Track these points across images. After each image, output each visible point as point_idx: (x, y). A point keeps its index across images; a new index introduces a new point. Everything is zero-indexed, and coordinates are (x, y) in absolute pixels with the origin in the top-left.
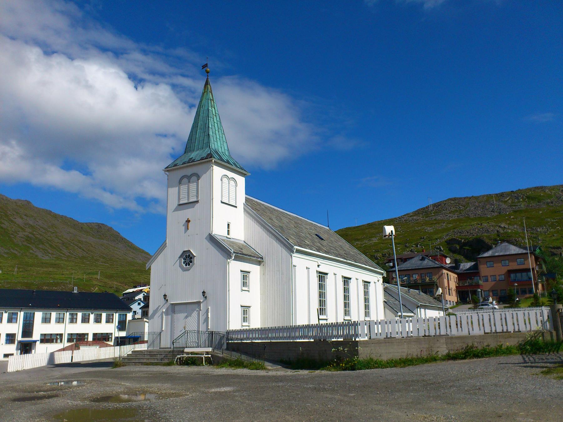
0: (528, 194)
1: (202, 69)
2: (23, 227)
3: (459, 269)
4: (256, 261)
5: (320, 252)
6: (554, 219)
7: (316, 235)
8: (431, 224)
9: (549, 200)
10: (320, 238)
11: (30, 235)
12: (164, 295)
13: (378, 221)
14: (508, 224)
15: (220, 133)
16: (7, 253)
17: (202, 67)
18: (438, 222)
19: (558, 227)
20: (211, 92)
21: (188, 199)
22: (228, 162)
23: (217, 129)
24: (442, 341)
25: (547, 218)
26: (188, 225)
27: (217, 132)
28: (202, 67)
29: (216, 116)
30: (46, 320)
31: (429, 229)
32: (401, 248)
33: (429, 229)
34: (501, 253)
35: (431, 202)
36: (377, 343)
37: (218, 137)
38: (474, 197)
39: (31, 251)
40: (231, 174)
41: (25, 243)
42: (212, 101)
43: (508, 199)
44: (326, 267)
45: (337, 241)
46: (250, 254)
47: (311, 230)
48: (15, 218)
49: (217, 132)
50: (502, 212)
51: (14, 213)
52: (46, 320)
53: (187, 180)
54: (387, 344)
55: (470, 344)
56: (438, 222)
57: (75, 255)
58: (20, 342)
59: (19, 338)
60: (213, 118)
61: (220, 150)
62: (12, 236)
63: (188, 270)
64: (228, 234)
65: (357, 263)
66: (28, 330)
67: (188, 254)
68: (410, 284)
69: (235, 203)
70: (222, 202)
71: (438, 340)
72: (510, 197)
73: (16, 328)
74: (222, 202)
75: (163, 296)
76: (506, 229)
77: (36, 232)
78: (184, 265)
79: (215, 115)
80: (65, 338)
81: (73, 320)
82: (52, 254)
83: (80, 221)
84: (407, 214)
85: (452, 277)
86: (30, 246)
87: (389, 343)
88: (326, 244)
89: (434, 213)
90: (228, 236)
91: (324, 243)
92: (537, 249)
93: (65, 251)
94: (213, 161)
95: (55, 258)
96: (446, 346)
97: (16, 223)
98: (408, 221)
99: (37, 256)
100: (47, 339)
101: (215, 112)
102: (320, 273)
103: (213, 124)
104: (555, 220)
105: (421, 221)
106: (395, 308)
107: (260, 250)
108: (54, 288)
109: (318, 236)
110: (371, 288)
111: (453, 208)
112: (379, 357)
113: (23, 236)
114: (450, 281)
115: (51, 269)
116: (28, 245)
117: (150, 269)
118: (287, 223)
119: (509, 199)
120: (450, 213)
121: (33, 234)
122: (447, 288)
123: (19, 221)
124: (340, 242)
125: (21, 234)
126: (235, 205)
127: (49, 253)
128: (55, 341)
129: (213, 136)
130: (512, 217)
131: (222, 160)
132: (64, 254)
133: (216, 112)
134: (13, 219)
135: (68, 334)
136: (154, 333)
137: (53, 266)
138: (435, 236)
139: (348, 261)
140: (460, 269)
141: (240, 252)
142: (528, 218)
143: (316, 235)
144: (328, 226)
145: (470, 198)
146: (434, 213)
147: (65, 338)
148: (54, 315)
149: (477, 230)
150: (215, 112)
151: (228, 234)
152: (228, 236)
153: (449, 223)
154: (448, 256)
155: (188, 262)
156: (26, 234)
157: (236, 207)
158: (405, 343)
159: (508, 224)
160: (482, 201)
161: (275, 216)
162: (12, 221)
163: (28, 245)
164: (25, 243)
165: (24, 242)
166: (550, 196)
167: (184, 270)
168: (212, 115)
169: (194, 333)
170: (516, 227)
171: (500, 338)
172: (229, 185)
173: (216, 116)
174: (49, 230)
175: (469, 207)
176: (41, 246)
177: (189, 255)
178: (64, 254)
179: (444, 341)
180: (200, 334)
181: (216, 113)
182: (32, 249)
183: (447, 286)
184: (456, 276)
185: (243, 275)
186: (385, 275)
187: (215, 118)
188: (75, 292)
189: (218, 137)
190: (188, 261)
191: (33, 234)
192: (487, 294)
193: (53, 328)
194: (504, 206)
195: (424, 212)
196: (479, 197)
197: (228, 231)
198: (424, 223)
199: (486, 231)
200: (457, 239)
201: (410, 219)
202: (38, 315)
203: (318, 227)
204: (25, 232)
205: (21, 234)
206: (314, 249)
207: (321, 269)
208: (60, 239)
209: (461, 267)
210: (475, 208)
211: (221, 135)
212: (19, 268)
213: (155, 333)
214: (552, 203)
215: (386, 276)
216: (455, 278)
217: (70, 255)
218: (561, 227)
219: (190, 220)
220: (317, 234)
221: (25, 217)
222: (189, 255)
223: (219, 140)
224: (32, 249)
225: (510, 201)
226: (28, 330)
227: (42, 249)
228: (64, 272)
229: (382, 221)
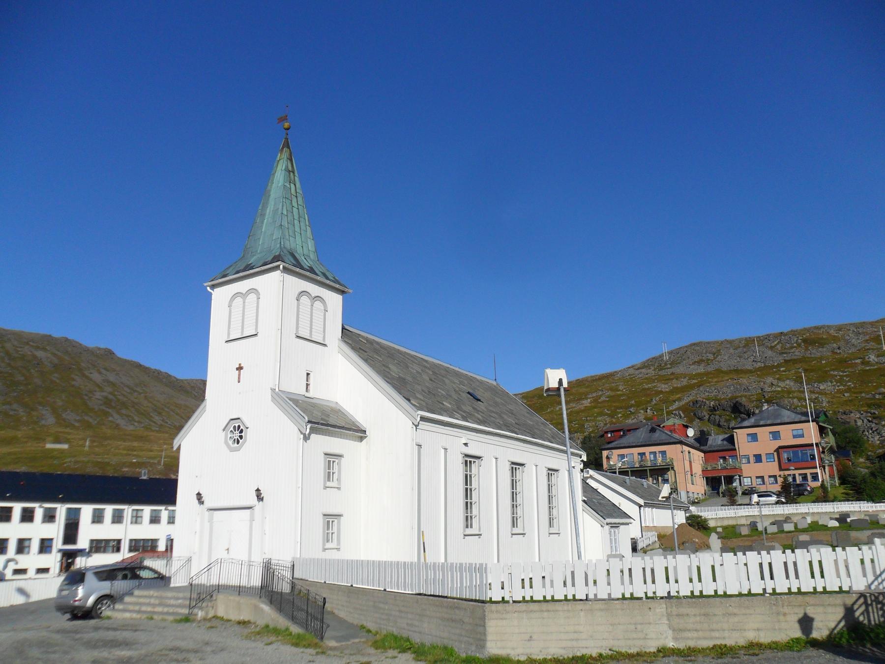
0: (804, 336)
1: (278, 123)
2: (101, 385)
3: (706, 445)
4: (355, 437)
5: (469, 422)
6: (843, 372)
7: (469, 393)
8: (668, 380)
9: (835, 344)
10: (474, 397)
11: (111, 397)
12: (256, 490)
13: (592, 377)
14: (778, 379)
15: (302, 224)
16: (78, 421)
17: (278, 121)
18: (677, 377)
19: (850, 384)
20: (290, 160)
21: (229, 334)
22: (311, 270)
23: (296, 217)
24: (658, 610)
25: (833, 370)
26: (239, 375)
27: (296, 222)
28: (278, 121)
29: (296, 197)
30: (98, 518)
31: (664, 387)
32: (623, 415)
33: (664, 387)
34: (769, 421)
35: (665, 349)
36: (524, 611)
37: (297, 229)
38: (727, 341)
39: (111, 419)
40: (315, 290)
41: (103, 407)
42: (292, 174)
43: (776, 343)
44: (479, 444)
45: (506, 402)
46: (343, 424)
47: (461, 386)
48: (91, 373)
49: (296, 222)
50: (768, 362)
51: (90, 366)
52: (98, 518)
53: (242, 300)
54: (546, 614)
55: (732, 405)
56: (677, 377)
57: (170, 425)
58: (60, 551)
59: (58, 545)
60: (291, 201)
61: (299, 250)
62: (86, 398)
63: (238, 450)
64: (307, 390)
65: (535, 438)
66: (71, 532)
67: (237, 425)
68: (635, 468)
69: (322, 339)
70: (298, 337)
71: (650, 608)
72: (779, 340)
73: (55, 531)
74: (298, 337)
75: (195, 496)
76: (774, 387)
77: (118, 392)
78: (230, 442)
79: (295, 195)
80: (125, 546)
81: (137, 519)
82: (139, 422)
83: (178, 377)
84: (632, 367)
85: (696, 458)
86: (110, 411)
87: (548, 611)
88: (483, 408)
89: (670, 364)
90: (307, 393)
91: (481, 406)
92: (820, 415)
93: (157, 418)
94: (281, 267)
95: (143, 427)
96: (667, 622)
97: (91, 380)
98: (634, 376)
99: (118, 425)
100: (98, 546)
101: (296, 190)
102: (467, 456)
103: (289, 209)
104: (845, 374)
105: (652, 376)
106: (601, 511)
107: (360, 417)
108: (138, 469)
109: (471, 395)
110: (562, 479)
111: (698, 357)
112: (529, 640)
113: (100, 398)
114: (693, 463)
115: (136, 444)
116: (107, 410)
117: (179, 448)
118: (418, 372)
119: (778, 343)
120: (693, 364)
121: (115, 395)
122: (689, 473)
123: (96, 376)
124: (511, 404)
125: (98, 395)
126: (322, 342)
127: (136, 422)
128: (102, 549)
129: (288, 228)
130: (782, 369)
131: (302, 268)
132: (155, 422)
133: (298, 191)
134: (89, 375)
135: (131, 540)
136: (178, 559)
137: (140, 438)
138: (673, 397)
139: (519, 436)
140: (708, 445)
141: (322, 422)
142: (806, 371)
143: (469, 393)
144: (495, 380)
145: (722, 342)
146: (670, 364)
147: (125, 546)
148: (109, 510)
149: (732, 388)
150: (296, 190)
151: (307, 390)
152: (307, 395)
153: (692, 377)
154: (689, 425)
155: (237, 439)
156: (105, 394)
157: (325, 345)
158: (582, 614)
159: (778, 379)
160: (739, 347)
161: (396, 361)
162: (87, 377)
163: (107, 410)
164: (103, 407)
165: (101, 405)
166: (835, 339)
167: (232, 450)
168: (290, 195)
169: (231, 563)
170: (788, 383)
171: (783, 607)
172: (312, 309)
173: (296, 197)
174: (135, 388)
175: (721, 355)
176: (124, 411)
177: (239, 427)
178: (155, 422)
179: (663, 610)
180: (240, 566)
181: (296, 192)
182: (112, 416)
183: (689, 470)
184: (702, 455)
185: (328, 461)
186: (585, 458)
187: (294, 200)
188: (145, 478)
189: (297, 229)
190: (237, 435)
191: (115, 395)
192: (748, 482)
193: (107, 531)
194: (769, 353)
195: (656, 363)
196: (733, 341)
197: (307, 385)
198: (656, 379)
199: (745, 389)
200: (704, 400)
201: (637, 372)
202: (87, 510)
203: (478, 380)
204: (103, 391)
205: (98, 395)
206: (458, 415)
207: (470, 451)
208: (151, 402)
209: (710, 442)
210: (729, 357)
211: (303, 227)
212: (92, 441)
213: (181, 558)
214: (839, 348)
215: (585, 460)
216: (701, 458)
217: (163, 424)
218: (853, 383)
219: (243, 367)
220: (471, 391)
221: (104, 372)
222: (239, 427)
223: (299, 234)
224: (112, 416)
225: (779, 347)
226: (71, 532)
227: (125, 415)
228: (152, 448)
229: (597, 376)
